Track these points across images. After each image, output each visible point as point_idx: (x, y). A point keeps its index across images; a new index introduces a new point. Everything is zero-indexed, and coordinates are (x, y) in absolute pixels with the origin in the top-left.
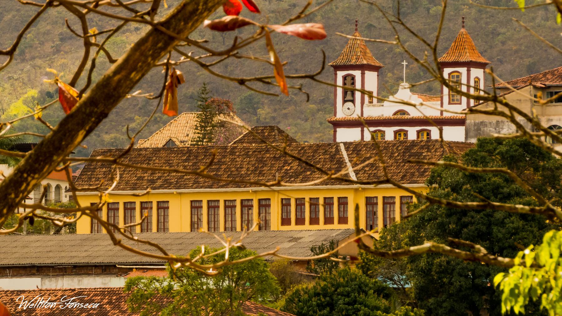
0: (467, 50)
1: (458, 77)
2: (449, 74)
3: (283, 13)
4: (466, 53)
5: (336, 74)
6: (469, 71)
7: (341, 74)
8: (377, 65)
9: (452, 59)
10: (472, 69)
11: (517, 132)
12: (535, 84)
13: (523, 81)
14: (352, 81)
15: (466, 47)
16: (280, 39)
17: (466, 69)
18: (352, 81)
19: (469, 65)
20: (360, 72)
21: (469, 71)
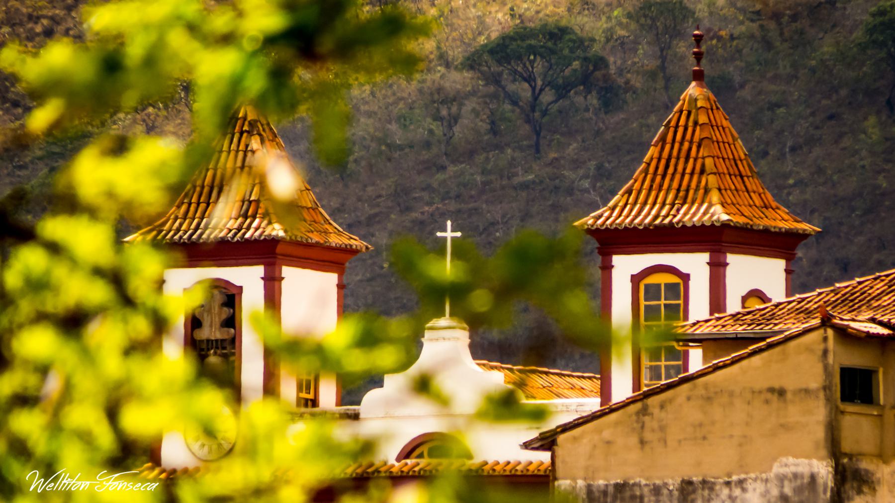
0: (712, 180)
1: (672, 289)
2: (636, 280)
3: (794, 18)
4: (707, 191)
5: (607, 268)
6: (717, 269)
7: (626, 266)
8: (335, 240)
9: (646, 216)
10: (731, 258)
11: (599, 491)
12: (844, 318)
13: (799, 311)
14: (226, 312)
15: (709, 162)
16: (779, 133)
17: (259, 271)
18: (226, 312)
19: (716, 241)
20: (705, 257)
21: (717, 269)
